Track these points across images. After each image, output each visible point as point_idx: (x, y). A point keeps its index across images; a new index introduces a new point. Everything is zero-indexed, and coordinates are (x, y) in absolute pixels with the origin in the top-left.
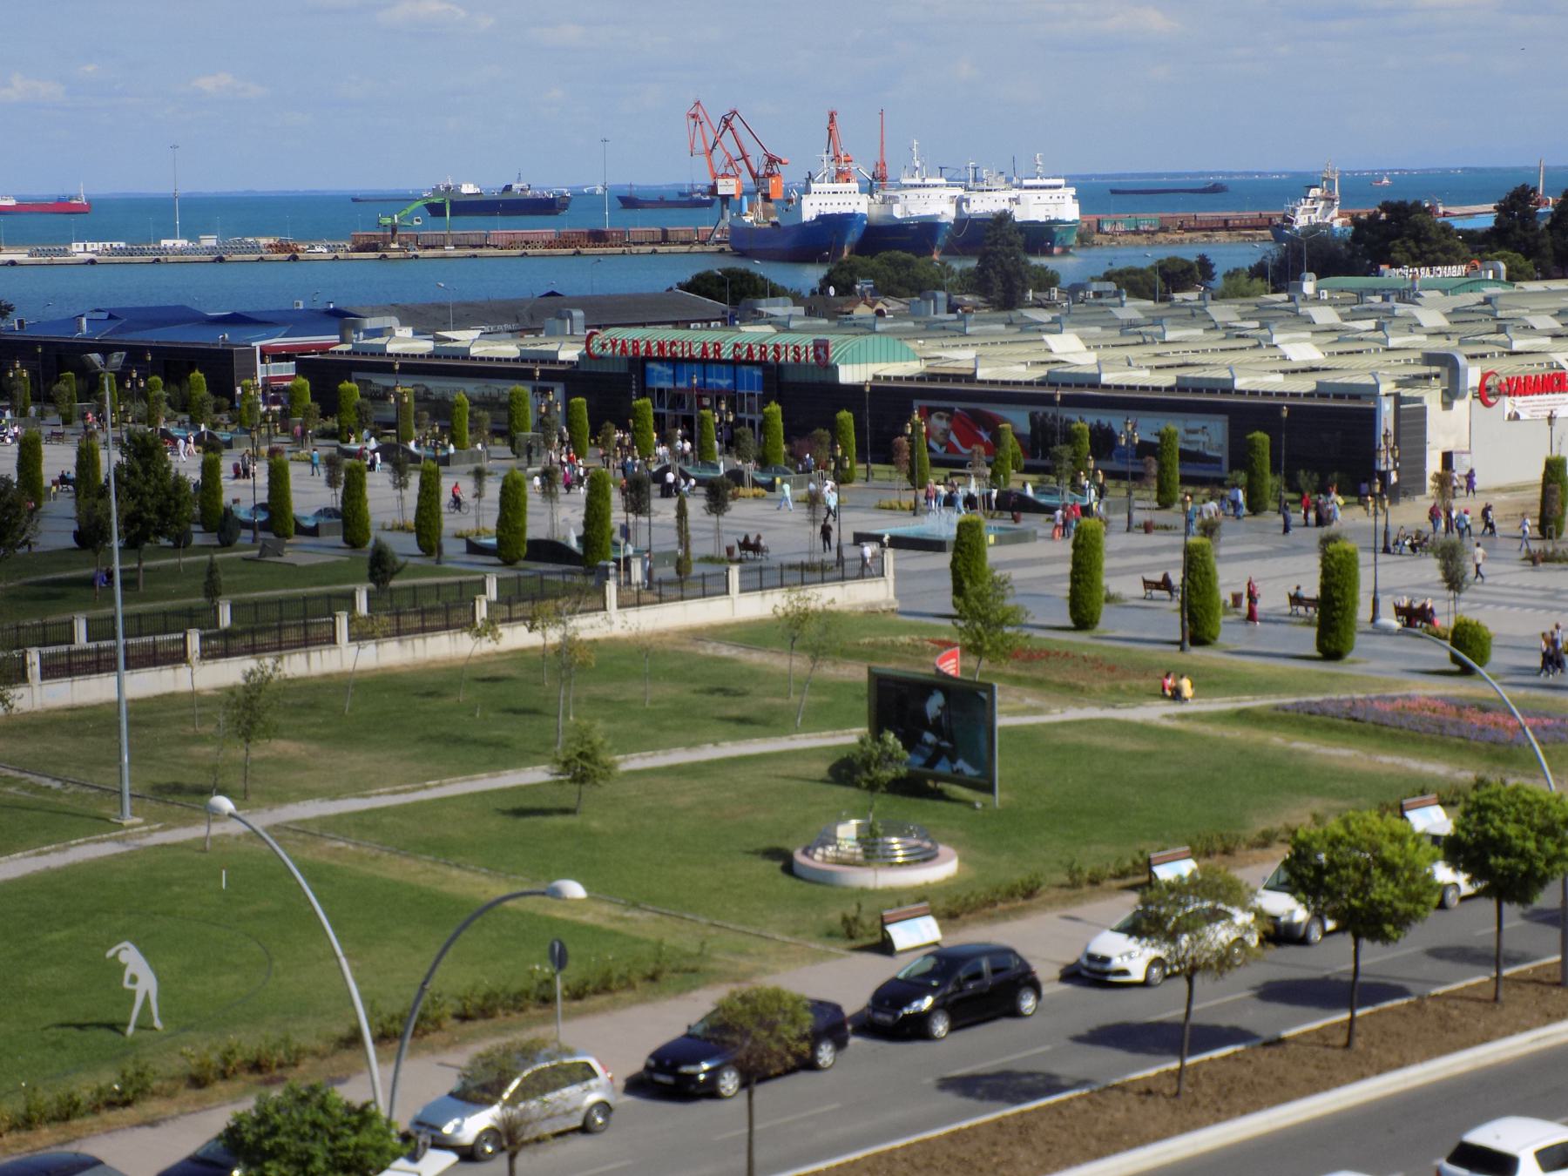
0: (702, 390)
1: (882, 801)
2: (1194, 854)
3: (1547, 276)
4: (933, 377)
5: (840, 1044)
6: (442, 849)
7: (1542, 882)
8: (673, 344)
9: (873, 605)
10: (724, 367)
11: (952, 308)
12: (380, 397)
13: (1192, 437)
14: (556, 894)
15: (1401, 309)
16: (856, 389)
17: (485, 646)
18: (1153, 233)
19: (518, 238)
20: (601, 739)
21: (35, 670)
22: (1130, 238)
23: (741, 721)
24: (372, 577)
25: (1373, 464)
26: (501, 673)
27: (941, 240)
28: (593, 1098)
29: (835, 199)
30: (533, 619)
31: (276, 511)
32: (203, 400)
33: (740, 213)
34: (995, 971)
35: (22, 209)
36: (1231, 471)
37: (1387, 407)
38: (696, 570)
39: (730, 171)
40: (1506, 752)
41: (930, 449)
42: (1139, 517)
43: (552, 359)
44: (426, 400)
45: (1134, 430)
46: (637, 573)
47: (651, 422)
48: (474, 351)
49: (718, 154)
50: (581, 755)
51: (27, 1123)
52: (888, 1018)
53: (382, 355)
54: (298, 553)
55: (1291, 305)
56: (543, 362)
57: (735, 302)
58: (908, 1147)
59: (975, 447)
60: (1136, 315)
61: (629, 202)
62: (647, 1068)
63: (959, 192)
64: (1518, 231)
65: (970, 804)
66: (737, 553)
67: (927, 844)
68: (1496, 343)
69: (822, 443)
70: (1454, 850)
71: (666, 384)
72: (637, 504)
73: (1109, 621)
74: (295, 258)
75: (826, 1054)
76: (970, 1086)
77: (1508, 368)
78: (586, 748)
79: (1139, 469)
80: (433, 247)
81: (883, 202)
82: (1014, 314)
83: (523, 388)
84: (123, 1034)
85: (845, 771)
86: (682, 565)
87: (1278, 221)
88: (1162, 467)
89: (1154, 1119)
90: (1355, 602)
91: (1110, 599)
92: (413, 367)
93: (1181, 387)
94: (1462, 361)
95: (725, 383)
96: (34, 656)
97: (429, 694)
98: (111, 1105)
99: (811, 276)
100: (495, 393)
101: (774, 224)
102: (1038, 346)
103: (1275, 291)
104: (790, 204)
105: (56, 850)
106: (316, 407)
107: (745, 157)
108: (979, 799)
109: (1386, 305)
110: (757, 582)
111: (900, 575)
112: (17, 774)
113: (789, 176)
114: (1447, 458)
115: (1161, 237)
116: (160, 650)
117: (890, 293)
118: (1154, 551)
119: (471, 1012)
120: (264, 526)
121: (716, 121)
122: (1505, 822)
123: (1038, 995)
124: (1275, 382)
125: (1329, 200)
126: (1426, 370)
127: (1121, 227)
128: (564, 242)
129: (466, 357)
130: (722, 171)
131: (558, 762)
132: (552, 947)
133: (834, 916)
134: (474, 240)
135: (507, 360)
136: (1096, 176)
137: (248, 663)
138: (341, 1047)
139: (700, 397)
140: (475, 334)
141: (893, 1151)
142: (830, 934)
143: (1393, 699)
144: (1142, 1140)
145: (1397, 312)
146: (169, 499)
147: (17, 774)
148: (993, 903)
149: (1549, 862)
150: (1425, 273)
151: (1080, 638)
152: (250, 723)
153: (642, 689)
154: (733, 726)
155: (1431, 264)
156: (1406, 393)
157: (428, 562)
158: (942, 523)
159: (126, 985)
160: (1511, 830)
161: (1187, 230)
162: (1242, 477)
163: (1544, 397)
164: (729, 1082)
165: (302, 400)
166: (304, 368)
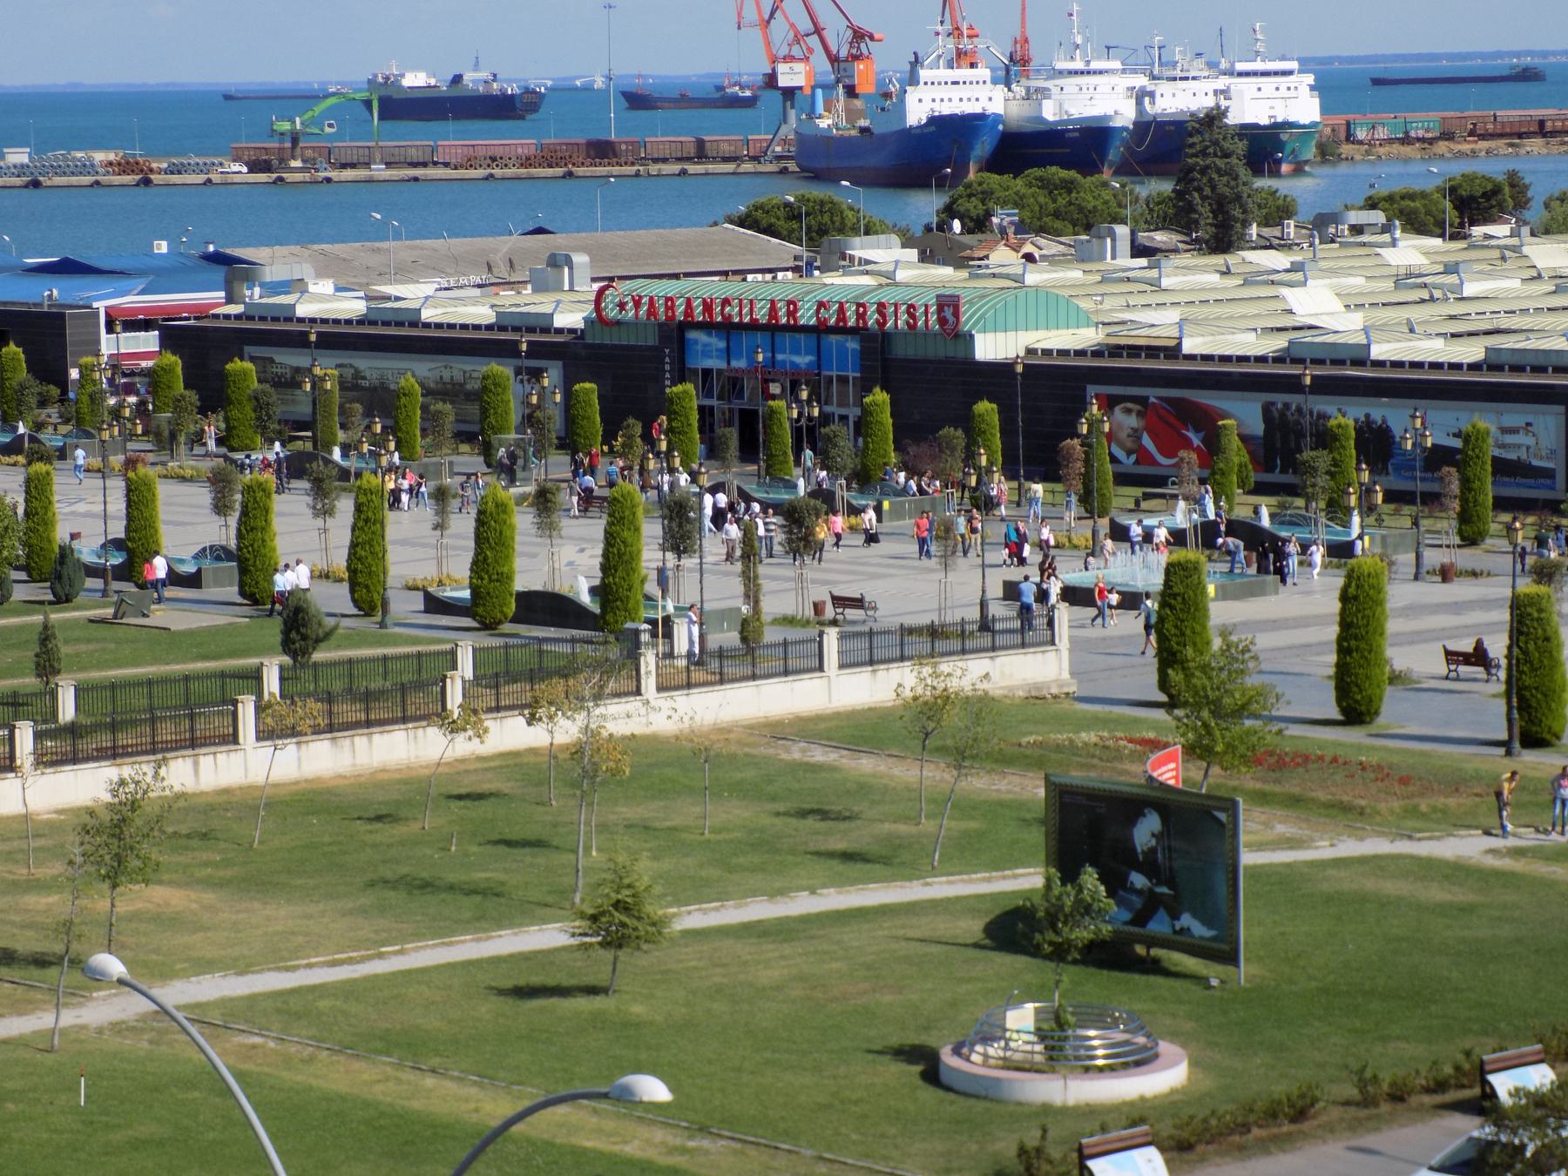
0: (768, 373)
4: (1116, 351)
8: (726, 302)
9: (1037, 687)
11: (1138, 251)
12: (288, 383)
13: (1509, 439)
14: (625, 1098)
16: (1001, 370)
17: (463, 746)
18: (1431, 141)
19: (481, 152)
20: (646, 880)
22: (1396, 149)
23: (848, 857)
26: (485, 787)
27: (1115, 153)
29: (956, 92)
32: (22, 387)
33: (812, 115)
38: (771, 635)
39: (796, 51)
41: (1114, 460)
42: (1433, 558)
43: (542, 325)
44: (356, 387)
46: (684, 636)
47: (694, 418)
48: (427, 315)
49: (779, 27)
50: (617, 905)
53: (289, 319)
56: (531, 330)
59: (1183, 453)
61: (637, 100)
63: (1141, 81)
66: (829, 612)
67: (1141, 1040)
73: (1394, 710)
74: (147, 182)
79: (1434, 487)
80: (353, 166)
82: (1232, 259)
83: (501, 369)
86: (748, 629)
88: (1466, 483)
93: (1492, 363)
95: (804, 360)
97: (379, 818)
99: (925, 205)
100: (459, 377)
104: (889, 99)
106: (193, 397)
107: (818, 31)
108: (1214, 972)
113: (883, 62)
115: (1442, 147)
117: (1041, 230)
118: (1457, 607)
127: (1381, 133)
130: (784, 51)
134: (414, 155)
135: (477, 327)
136: (1340, 59)
139: (766, 381)
148: (1245, 1128)
151: (1352, 736)
153: (698, 809)
154: (838, 866)
161: (1483, 137)
166: (173, 337)
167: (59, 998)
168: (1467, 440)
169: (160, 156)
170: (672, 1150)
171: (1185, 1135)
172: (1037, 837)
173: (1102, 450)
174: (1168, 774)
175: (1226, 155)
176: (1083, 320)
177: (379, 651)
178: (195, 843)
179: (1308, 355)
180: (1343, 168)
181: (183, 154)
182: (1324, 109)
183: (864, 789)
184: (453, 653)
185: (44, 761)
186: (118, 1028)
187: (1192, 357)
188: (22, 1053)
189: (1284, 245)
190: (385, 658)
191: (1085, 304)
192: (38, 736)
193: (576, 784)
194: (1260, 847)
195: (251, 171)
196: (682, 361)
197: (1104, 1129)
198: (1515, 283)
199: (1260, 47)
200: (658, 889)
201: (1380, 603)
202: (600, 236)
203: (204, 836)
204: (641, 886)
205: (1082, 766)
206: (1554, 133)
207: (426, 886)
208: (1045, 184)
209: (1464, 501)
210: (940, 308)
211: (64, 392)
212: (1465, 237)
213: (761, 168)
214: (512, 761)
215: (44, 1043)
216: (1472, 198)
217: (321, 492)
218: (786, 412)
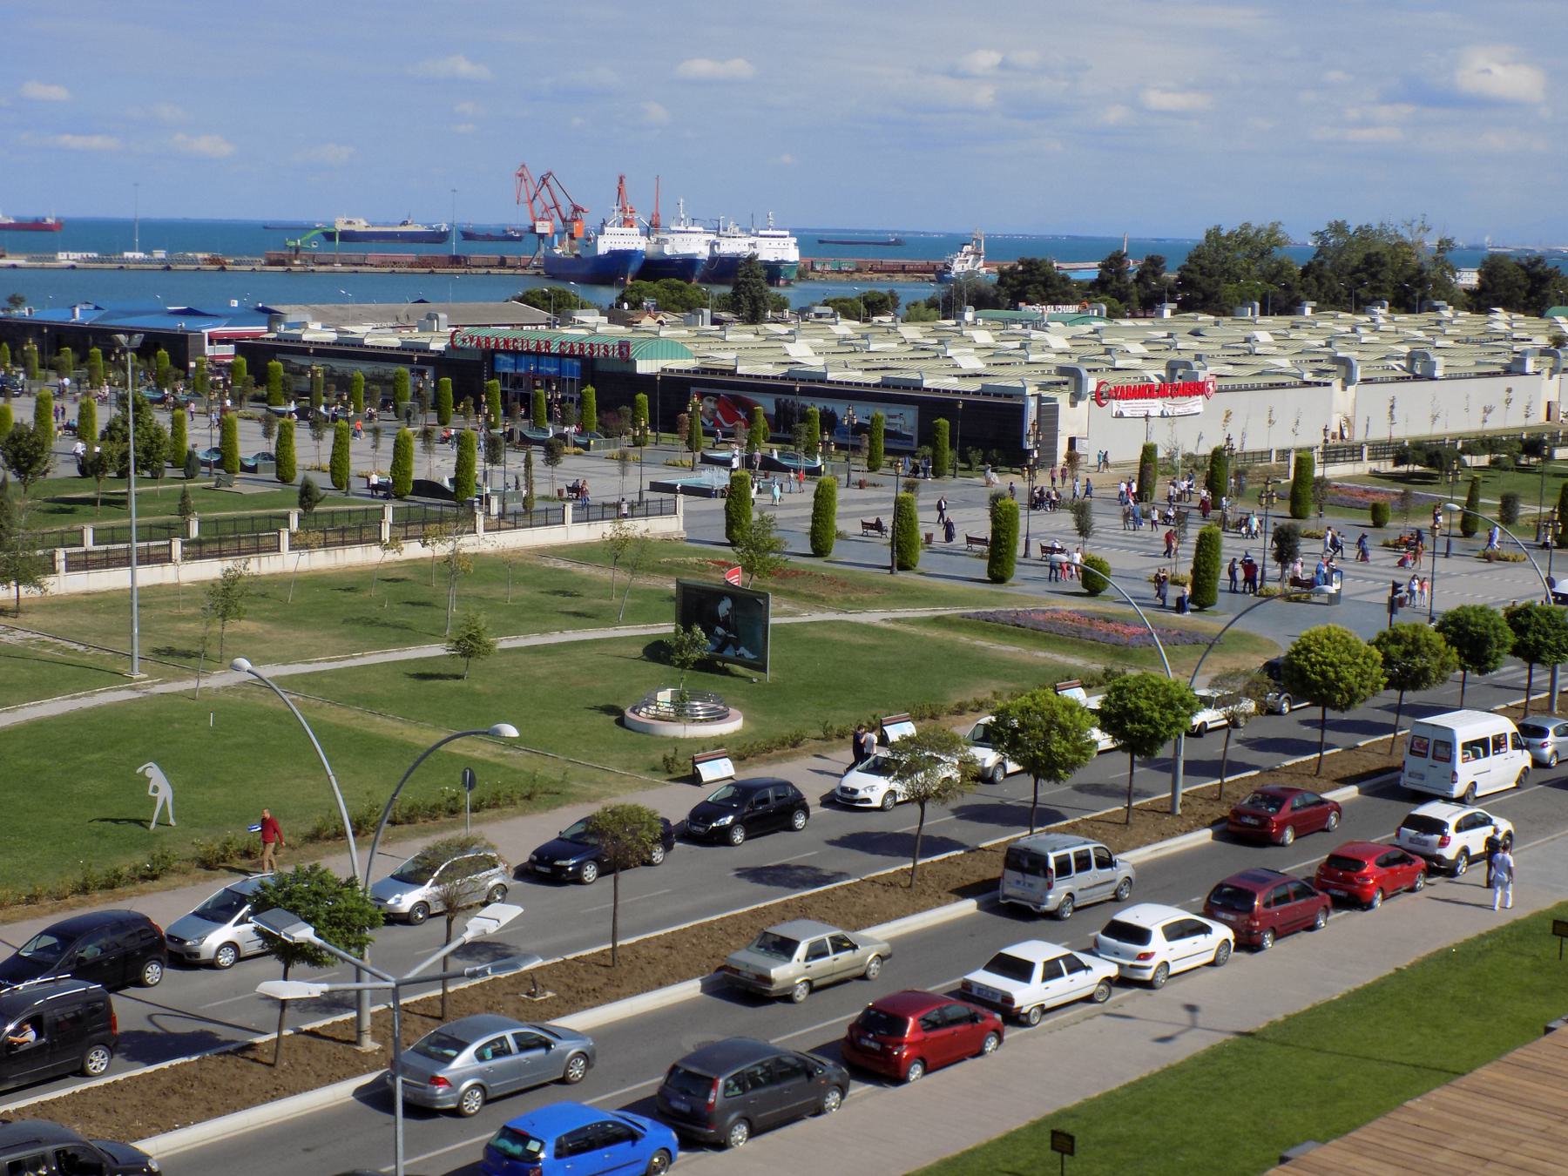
0: (536, 375)
1: (687, 674)
2: (916, 718)
3: (1134, 316)
4: (705, 371)
5: (668, 847)
6: (368, 702)
7: (1163, 741)
8: (515, 340)
9: (667, 534)
10: (552, 359)
11: (715, 322)
12: (300, 372)
13: (892, 421)
14: (496, 734)
15: (1035, 335)
16: (649, 378)
17: (391, 556)
18: (851, 272)
19: (389, 259)
20: (483, 625)
21: (61, 565)
22: (835, 275)
23: (576, 614)
24: (301, 504)
25: (1021, 443)
26: (401, 576)
27: (699, 271)
28: (495, 881)
29: (623, 239)
30: (426, 537)
31: (225, 458)
32: (168, 371)
33: (552, 247)
34: (778, 798)
35: (20, 227)
36: (919, 446)
37: (1032, 404)
38: (538, 506)
39: (546, 216)
40: (1121, 650)
41: (703, 424)
42: (856, 477)
43: (424, 348)
44: (331, 376)
45: (851, 414)
46: (495, 507)
47: (499, 397)
48: (367, 341)
49: (538, 204)
50: (469, 636)
51: (84, 889)
52: (701, 830)
53: (299, 341)
54: (242, 485)
55: (958, 328)
56: (418, 351)
57: (556, 313)
58: (722, 920)
59: (738, 423)
60: (849, 332)
61: (468, 236)
62: (531, 861)
63: (712, 237)
64: (1114, 283)
65: (750, 680)
66: (566, 494)
67: (721, 707)
68: (1104, 362)
69: (626, 416)
70: (1109, 719)
71: (509, 370)
72: (493, 458)
73: (837, 550)
74: (223, 269)
75: (658, 855)
76: (757, 875)
77: (1114, 380)
78: (473, 632)
79: (857, 443)
80: (325, 264)
81: (656, 243)
82: (759, 327)
83: (404, 369)
84: (148, 828)
85: (657, 651)
86: (527, 502)
87: (941, 267)
88: (872, 441)
89: (895, 903)
90: (1016, 543)
91: (840, 535)
92: (323, 351)
93: (885, 384)
94: (1084, 373)
95: (552, 370)
96: (60, 554)
97: (349, 590)
98: (144, 878)
99: (609, 295)
100: (382, 373)
101: (577, 255)
102: (779, 351)
103: (944, 318)
104: (590, 242)
105: (85, 696)
106: (252, 378)
107: (556, 206)
108: (755, 675)
109: (1025, 331)
110: (587, 513)
111: (687, 514)
112: (51, 640)
113: (588, 221)
114: (1072, 441)
115: (856, 275)
116: (153, 552)
117: (666, 310)
118: (866, 501)
119: (399, 818)
120: (219, 464)
121: (537, 179)
122: (1139, 698)
123: (807, 815)
124: (952, 383)
125: (977, 254)
126: (1059, 379)
127: (828, 268)
128: (422, 263)
129: (361, 345)
130: (539, 216)
131: (451, 641)
132: (465, 773)
133: (657, 757)
134: (355, 260)
135: (392, 348)
136: (807, 230)
137: (229, 563)
138: (1056, 911)
139: (534, 380)
140: (369, 329)
141: (712, 923)
142: (654, 769)
143: (1044, 612)
144: (887, 918)
145: (1032, 337)
146: (152, 442)
147: (51, 640)
148: (769, 750)
149: (1169, 728)
150: (1050, 309)
151: (818, 562)
152: (226, 607)
153: (504, 590)
154: (573, 619)
155: (1055, 303)
156: (1045, 394)
157: (337, 493)
158: (717, 478)
159: (150, 793)
160: (1143, 704)
161: (876, 272)
162: (928, 450)
163: (1140, 401)
164: (590, 872)
165: (240, 373)
166: (242, 349)
167: (198, 673)
168: (873, 420)
169: (229, 255)
170: (496, 755)
171: (743, 752)
172: (671, 607)
173: (700, 419)
174: (736, 579)
175: (757, 277)
176: (688, 355)
177: (346, 507)
178: (260, 599)
179: (798, 377)
180: (808, 285)
181: (242, 256)
182: (801, 255)
183: (584, 582)
184: (383, 510)
185: (186, 557)
186: (226, 689)
187: (742, 375)
188: (182, 700)
189: (785, 322)
190: (350, 511)
191: (690, 347)
192: (183, 544)
193: (446, 575)
194: (776, 615)
195: (1396, 465)
196: (493, 368)
197: (704, 749)
198: (895, 345)
199: (771, 223)
200: (489, 629)
201: (833, 499)
202: (451, 305)
203: (263, 596)
204: (481, 628)
205: (689, 574)
206: (909, 272)
207: (371, 623)
208: (669, 287)
209: (871, 450)
210: (620, 348)
211: (187, 373)
212: (870, 321)
213: (526, 272)
214: (413, 564)
215: (190, 695)
216: (873, 303)
217: (314, 425)
218: (544, 395)
